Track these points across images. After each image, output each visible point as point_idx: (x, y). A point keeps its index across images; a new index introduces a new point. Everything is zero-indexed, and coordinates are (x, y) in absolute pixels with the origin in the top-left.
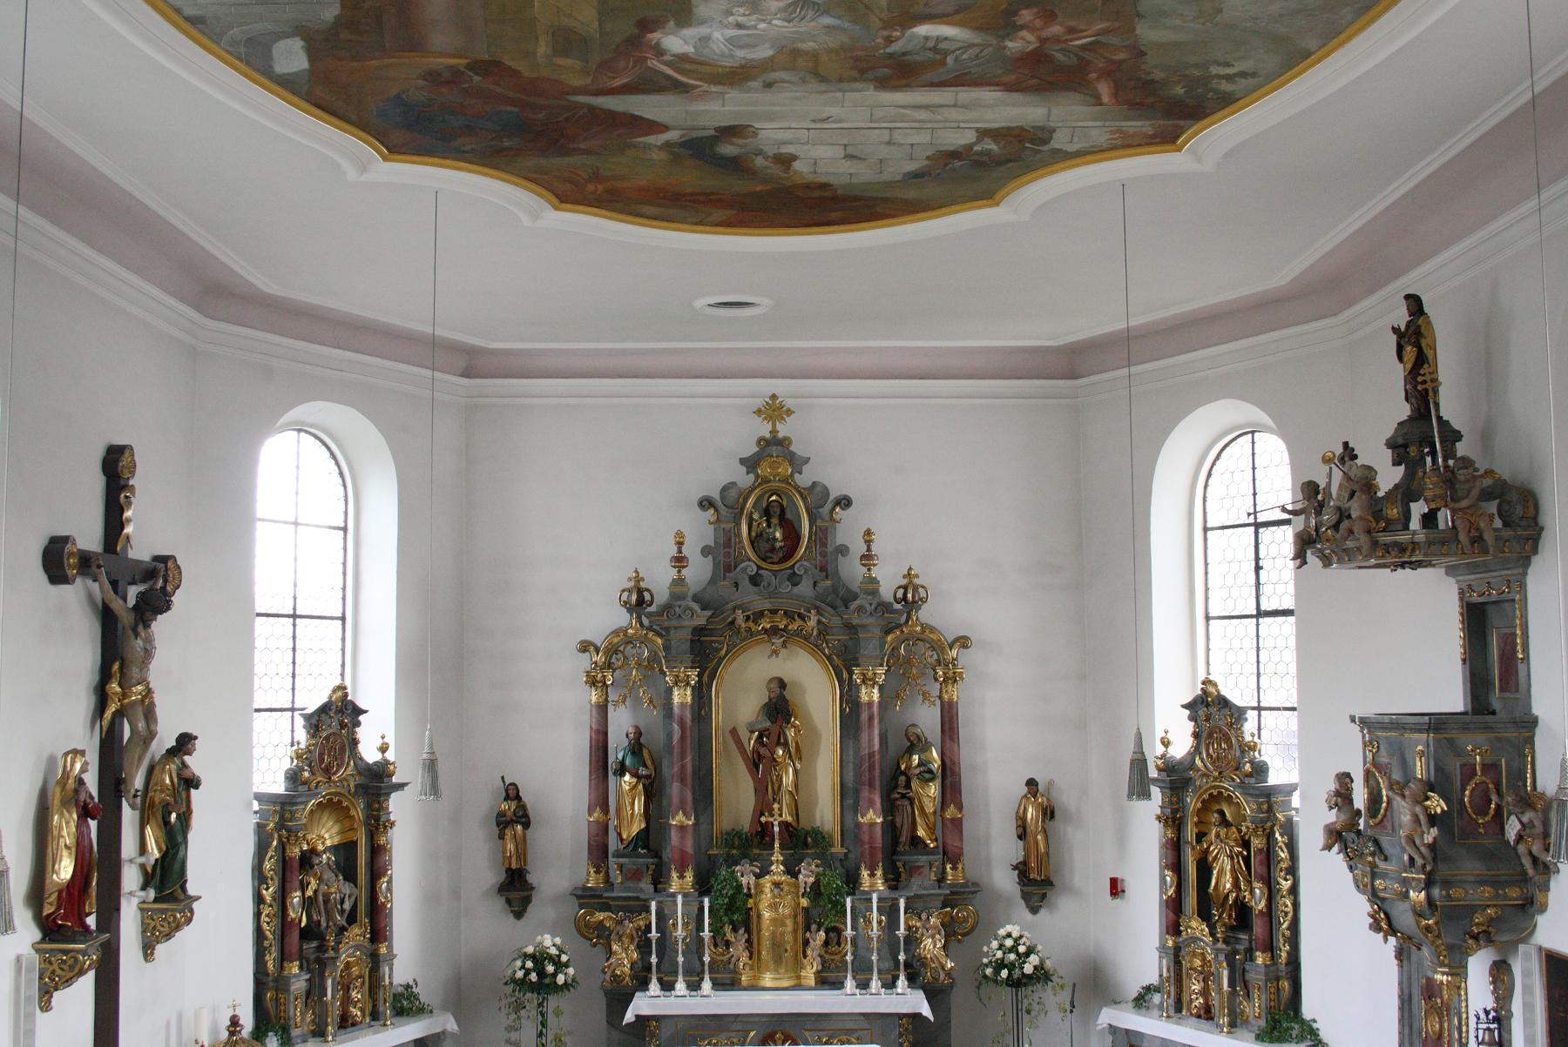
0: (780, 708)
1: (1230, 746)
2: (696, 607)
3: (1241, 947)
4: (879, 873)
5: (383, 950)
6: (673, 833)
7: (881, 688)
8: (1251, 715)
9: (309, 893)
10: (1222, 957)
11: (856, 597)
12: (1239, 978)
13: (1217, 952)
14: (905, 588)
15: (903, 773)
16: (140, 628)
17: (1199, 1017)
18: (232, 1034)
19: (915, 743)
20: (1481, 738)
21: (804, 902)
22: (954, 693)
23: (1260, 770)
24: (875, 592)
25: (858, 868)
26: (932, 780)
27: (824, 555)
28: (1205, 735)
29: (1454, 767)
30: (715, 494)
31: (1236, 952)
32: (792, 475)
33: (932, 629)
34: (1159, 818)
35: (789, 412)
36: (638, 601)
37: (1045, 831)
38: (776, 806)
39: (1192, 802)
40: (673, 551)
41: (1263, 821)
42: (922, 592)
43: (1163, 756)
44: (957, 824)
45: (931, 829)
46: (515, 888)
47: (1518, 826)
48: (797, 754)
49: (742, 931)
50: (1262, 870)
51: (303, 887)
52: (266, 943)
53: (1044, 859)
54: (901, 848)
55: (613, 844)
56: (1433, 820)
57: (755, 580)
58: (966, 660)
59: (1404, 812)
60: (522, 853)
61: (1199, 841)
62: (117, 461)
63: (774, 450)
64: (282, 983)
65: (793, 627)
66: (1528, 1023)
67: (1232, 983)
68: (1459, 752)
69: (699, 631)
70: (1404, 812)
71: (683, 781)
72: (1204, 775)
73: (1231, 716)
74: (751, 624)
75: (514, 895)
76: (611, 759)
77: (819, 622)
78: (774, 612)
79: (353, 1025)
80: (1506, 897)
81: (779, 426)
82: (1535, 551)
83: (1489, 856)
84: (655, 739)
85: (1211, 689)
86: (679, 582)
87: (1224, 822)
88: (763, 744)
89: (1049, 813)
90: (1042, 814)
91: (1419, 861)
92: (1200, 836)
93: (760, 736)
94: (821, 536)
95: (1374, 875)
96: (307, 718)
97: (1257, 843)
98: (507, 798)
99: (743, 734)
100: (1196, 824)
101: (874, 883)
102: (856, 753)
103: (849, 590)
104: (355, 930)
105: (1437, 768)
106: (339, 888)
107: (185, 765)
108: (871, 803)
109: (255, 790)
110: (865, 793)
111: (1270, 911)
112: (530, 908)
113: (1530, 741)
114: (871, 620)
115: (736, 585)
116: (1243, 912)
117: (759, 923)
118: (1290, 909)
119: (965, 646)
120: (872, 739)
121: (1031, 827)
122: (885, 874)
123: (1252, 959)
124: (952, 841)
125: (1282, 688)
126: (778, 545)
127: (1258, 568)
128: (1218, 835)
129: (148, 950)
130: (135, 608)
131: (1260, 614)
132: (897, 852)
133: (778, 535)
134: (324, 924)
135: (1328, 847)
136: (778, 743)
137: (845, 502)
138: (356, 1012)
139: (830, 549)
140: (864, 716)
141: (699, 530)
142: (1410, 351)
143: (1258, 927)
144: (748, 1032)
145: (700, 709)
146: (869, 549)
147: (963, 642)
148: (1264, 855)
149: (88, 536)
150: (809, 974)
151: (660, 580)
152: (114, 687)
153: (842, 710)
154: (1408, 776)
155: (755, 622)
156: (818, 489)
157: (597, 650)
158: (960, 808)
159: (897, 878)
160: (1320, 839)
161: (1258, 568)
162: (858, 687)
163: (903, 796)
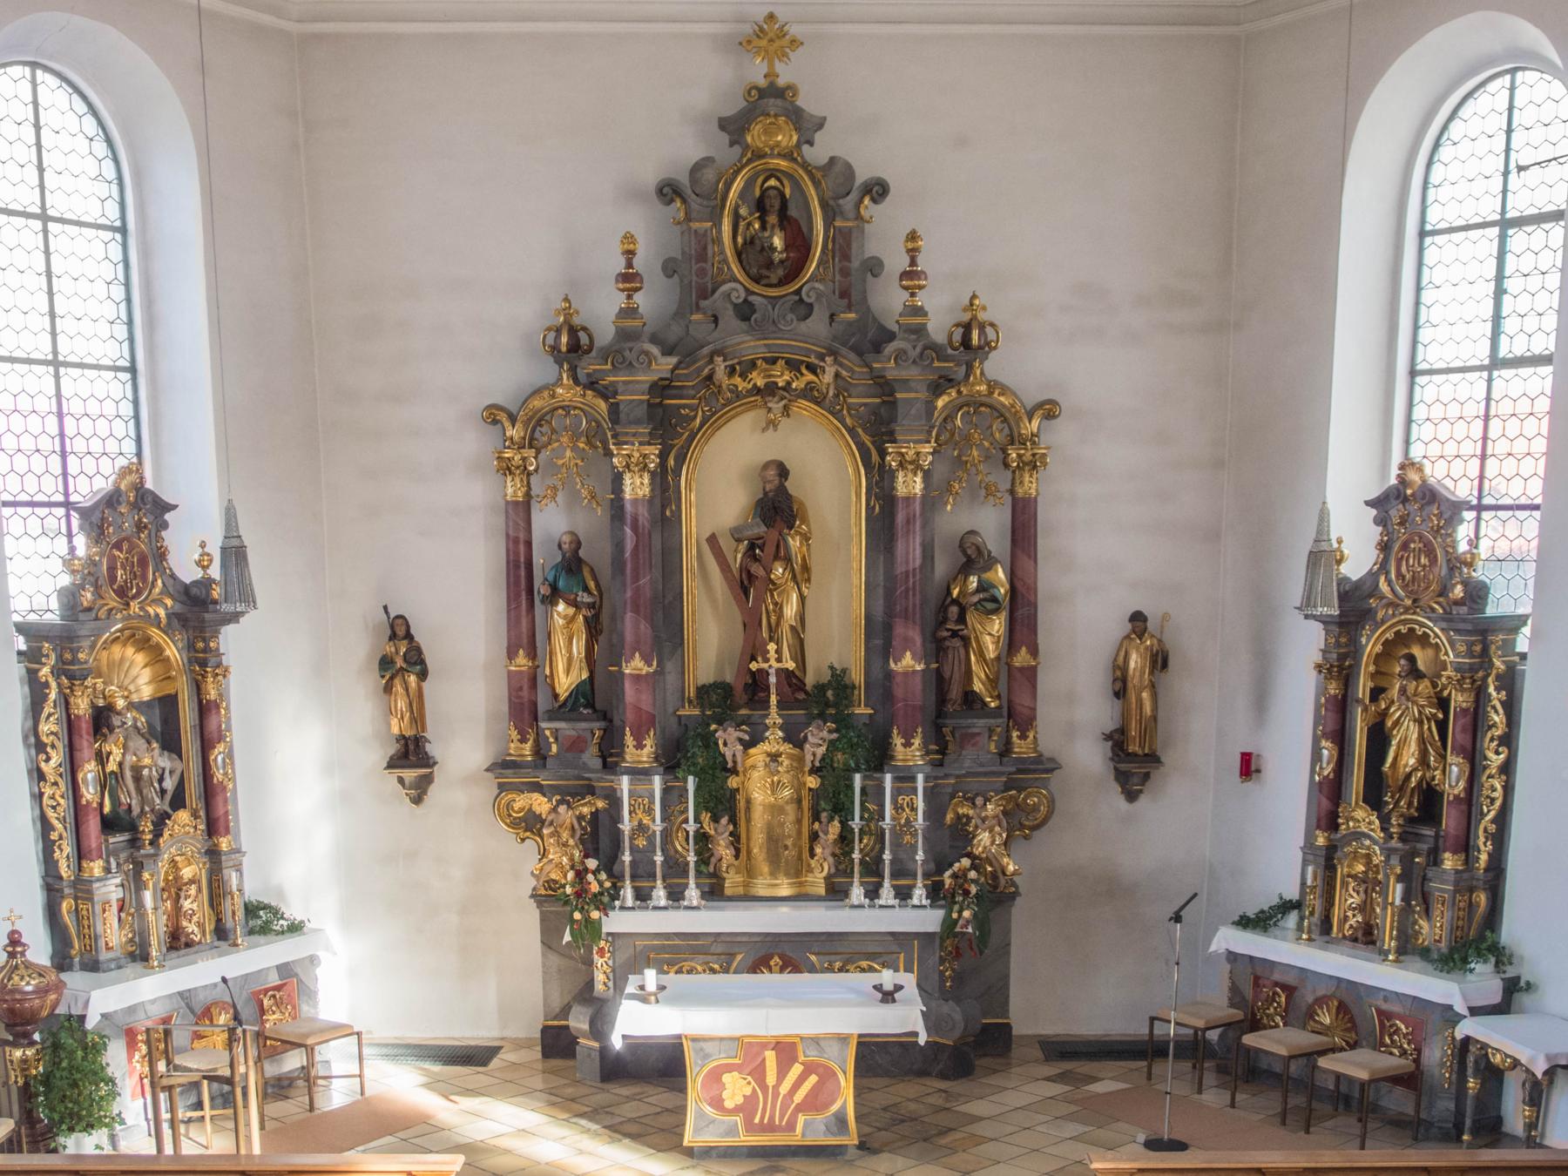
0: (777, 506)
2: (655, 350)
4: (917, 742)
5: (224, 844)
6: (628, 686)
7: (927, 475)
8: (1469, 515)
9: (112, 766)
10: (1395, 860)
11: (891, 336)
12: (1419, 895)
13: (1388, 853)
14: (967, 328)
15: (955, 602)
17: (1355, 940)
18: (12, 955)
19: (972, 558)
21: (812, 782)
22: (1029, 485)
23: (1477, 594)
24: (920, 331)
25: (888, 735)
26: (996, 611)
27: (845, 273)
28: (1397, 546)
30: (684, 179)
31: (1415, 853)
32: (798, 145)
33: (1005, 390)
34: (1319, 667)
35: (795, 43)
36: (571, 345)
37: (1153, 686)
38: (772, 647)
39: (1371, 645)
40: (619, 265)
41: (1473, 669)
44: (1030, 674)
45: (992, 682)
46: (411, 755)
48: (802, 574)
49: (724, 821)
50: (1464, 739)
51: (102, 758)
52: (54, 836)
54: (950, 708)
55: (543, 703)
57: (745, 311)
58: (1059, 438)
60: (418, 715)
63: (772, 104)
64: (82, 889)
67: (1406, 897)
69: (661, 388)
71: (636, 610)
72: (1390, 604)
73: (1440, 516)
74: (737, 380)
75: (410, 774)
76: (542, 589)
77: (837, 375)
78: (774, 361)
79: (188, 945)
81: (779, 67)
84: (597, 553)
85: (1413, 476)
86: (629, 312)
87: (1414, 673)
88: (756, 559)
89: (1160, 661)
90: (1148, 658)
92: (1376, 693)
93: (752, 547)
94: (842, 245)
96: (85, 513)
97: (1459, 700)
98: (393, 637)
99: (726, 544)
100: (1373, 676)
101: (910, 752)
103: (882, 328)
104: (183, 816)
106: (154, 759)
108: (907, 644)
109: (16, 618)
110: (900, 629)
111: (1469, 801)
112: (433, 790)
114: (911, 372)
115: (716, 319)
116: (1430, 799)
117: (748, 809)
118: (1498, 794)
120: (909, 551)
121: (1134, 680)
122: (925, 744)
124: (1022, 700)
125: (1521, 473)
126: (777, 257)
127: (1500, 292)
128: (1403, 691)
131: (1496, 363)
132: (947, 710)
133: (778, 242)
134: (136, 811)
136: (776, 557)
137: (878, 190)
138: (191, 927)
140: (900, 518)
141: (654, 236)
143: (1450, 820)
144: (732, 955)
145: (664, 507)
146: (913, 262)
147: (1049, 410)
148: (1469, 719)
150: (817, 881)
151: (602, 310)
156: (837, 168)
157: (513, 419)
158: (1034, 651)
159: (943, 751)
161: (1500, 292)
162: (892, 475)
163: (955, 634)
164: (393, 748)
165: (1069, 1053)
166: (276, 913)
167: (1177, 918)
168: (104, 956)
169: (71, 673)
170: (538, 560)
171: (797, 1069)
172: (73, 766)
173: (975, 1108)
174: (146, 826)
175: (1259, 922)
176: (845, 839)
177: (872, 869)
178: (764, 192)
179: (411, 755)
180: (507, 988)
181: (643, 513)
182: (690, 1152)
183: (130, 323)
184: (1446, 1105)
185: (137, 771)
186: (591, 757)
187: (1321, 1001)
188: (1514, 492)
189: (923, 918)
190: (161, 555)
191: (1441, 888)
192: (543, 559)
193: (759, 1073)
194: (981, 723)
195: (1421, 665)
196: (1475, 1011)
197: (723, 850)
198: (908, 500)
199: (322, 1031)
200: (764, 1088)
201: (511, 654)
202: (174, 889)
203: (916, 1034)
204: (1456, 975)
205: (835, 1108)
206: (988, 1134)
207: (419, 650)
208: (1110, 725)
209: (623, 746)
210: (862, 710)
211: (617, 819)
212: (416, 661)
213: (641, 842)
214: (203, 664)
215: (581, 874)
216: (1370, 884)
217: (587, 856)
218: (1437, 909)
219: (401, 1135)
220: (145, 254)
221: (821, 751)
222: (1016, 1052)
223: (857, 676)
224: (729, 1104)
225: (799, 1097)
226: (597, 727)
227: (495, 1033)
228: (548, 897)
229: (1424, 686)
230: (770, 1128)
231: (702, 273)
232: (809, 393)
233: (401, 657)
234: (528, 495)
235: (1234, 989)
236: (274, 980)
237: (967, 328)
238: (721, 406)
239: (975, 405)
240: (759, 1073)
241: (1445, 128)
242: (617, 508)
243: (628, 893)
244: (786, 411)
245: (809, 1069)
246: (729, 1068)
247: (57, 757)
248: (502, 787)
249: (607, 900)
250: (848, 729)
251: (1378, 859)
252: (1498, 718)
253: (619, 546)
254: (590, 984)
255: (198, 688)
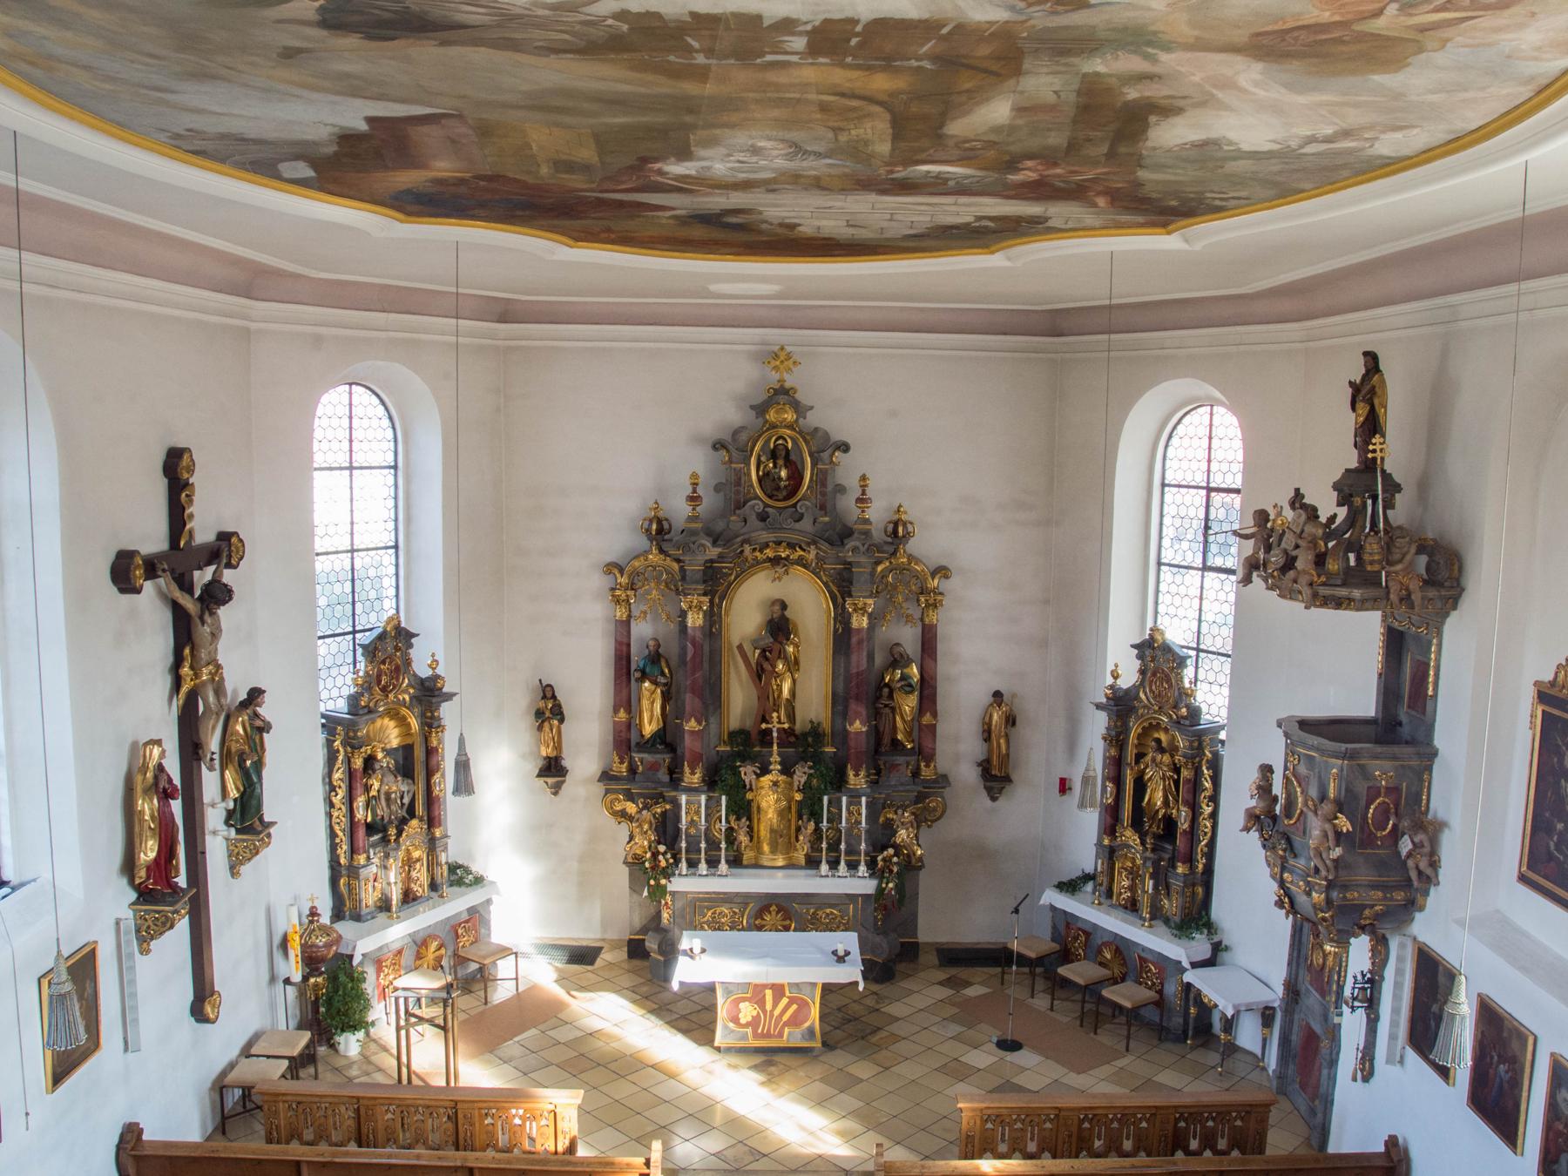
0: (779, 627)
1: (1171, 686)
3: (1167, 856)
4: (862, 773)
5: (438, 833)
6: (686, 736)
7: (870, 616)
9: (373, 793)
10: (1149, 864)
13: (1145, 859)
14: (896, 524)
15: (887, 685)
16: (207, 617)
19: (897, 660)
20: (1387, 764)
21: (798, 797)
23: (1195, 713)
24: (867, 533)
26: (911, 692)
27: (824, 494)
29: (1361, 787)
31: (1161, 859)
33: (918, 561)
34: (1105, 739)
36: (659, 531)
38: (775, 715)
39: (1134, 731)
41: (1193, 757)
42: (910, 528)
43: (1112, 687)
44: (932, 729)
45: (909, 734)
46: (553, 769)
47: (1410, 846)
48: (794, 665)
50: (1189, 797)
51: (367, 788)
53: (1005, 759)
56: (1339, 835)
57: (763, 517)
58: (951, 586)
59: (1316, 827)
60: (558, 746)
61: (1137, 762)
62: (177, 465)
63: (782, 398)
64: (353, 871)
65: (794, 556)
66: (1396, 997)
67: (1156, 887)
68: (1364, 772)
70: (1316, 827)
72: (1145, 707)
75: (550, 780)
79: (415, 899)
80: (1392, 899)
81: (786, 376)
82: (1455, 608)
83: (1381, 865)
84: (671, 649)
85: (1159, 638)
88: (767, 659)
89: (1011, 720)
90: (1003, 719)
91: (1324, 873)
92: (1140, 756)
93: (764, 651)
94: (821, 479)
95: (1283, 869)
98: (544, 697)
99: (747, 647)
102: (847, 669)
104: (414, 822)
105: (1347, 790)
106: (398, 786)
107: (256, 715)
109: (322, 709)
110: (853, 706)
111: (1192, 833)
113: (1429, 769)
114: (863, 559)
116: (1170, 823)
119: (947, 577)
120: (859, 661)
123: (1174, 867)
124: (927, 743)
126: (782, 484)
128: (1154, 760)
129: (234, 871)
130: (201, 599)
131: (1205, 568)
135: (1247, 829)
137: (844, 447)
139: (830, 488)
140: (854, 640)
142: (1363, 409)
143: (1180, 842)
147: (942, 571)
149: (151, 537)
150: (800, 856)
151: (678, 510)
152: (186, 670)
153: (836, 631)
154: (1323, 797)
155: (761, 551)
157: (622, 571)
158: (935, 715)
159: (878, 773)
160: (1241, 820)
162: (850, 615)
164: (540, 763)
165: (959, 958)
166: (467, 871)
167: (1016, 911)
168: (364, 911)
169: (352, 744)
170: (634, 658)
171: (785, 1001)
172: (351, 799)
173: (894, 1009)
174: (392, 831)
175: (1070, 887)
176: (817, 830)
177: (834, 847)
178: (776, 446)
179: (553, 769)
180: (608, 911)
181: (699, 634)
182: (718, 1049)
183: (396, 520)
184: (1178, 1021)
185: (388, 795)
186: (663, 776)
187: (1106, 944)
188: (1218, 645)
189: (862, 884)
190: (408, 662)
191: (1176, 884)
192: (637, 659)
193: (761, 1003)
194: (900, 760)
195: (1164, 744)
196: (1194, 965)
197: (743, 838)
198: (859, 630)
199: (493, 954)
200: (765, 1012)
201: (616, 711)
202: (409, 863)
203: (856, 983)
204: (1184, 941)
205: (807, 1025)
206: (902, 1034)
207: (560, 706)
208: (981, 757)
209: (682, 773)
210: (830, 749)
211: (678, 819)
212: (558, 713)
213: (693, 831)
214: (430, 726)
215: (655, 855)
216: (1134, 874)
217: (659, 843)
218: (1174, 896)
219: (542, 1027)
220: (408, 507)
221: (803, 780)
222: (923, 958)
223: (828, 730)
224: (743, 1021)
225: (785, 1018)
226: (667, 758)
227: (599, 936)
228: (635, 863)
229: (1166, 758)
230: (768, 1036)
231: (738, 492)
232: (801, 562)
233: (549, 709)
234: (629, 616)
235: (1054, 927)
236: (465, 916)
237: (896, 524)
238: (746, 569)
239: (902, 569)
240: (761, 1003)
241: (1175, 428)
242: (683, 627)
243: (683, 865)
244: (786, 572)
245: (792, 1001)
246: (744, 1000)
247: (341, 793)
248: (607, 792)
249: (667, 873)
250: (817, 758)
251: (1139, 862)
252: (1208, 785)
253: (683, 649)
254: (658, 915)
255: (426, 739)
